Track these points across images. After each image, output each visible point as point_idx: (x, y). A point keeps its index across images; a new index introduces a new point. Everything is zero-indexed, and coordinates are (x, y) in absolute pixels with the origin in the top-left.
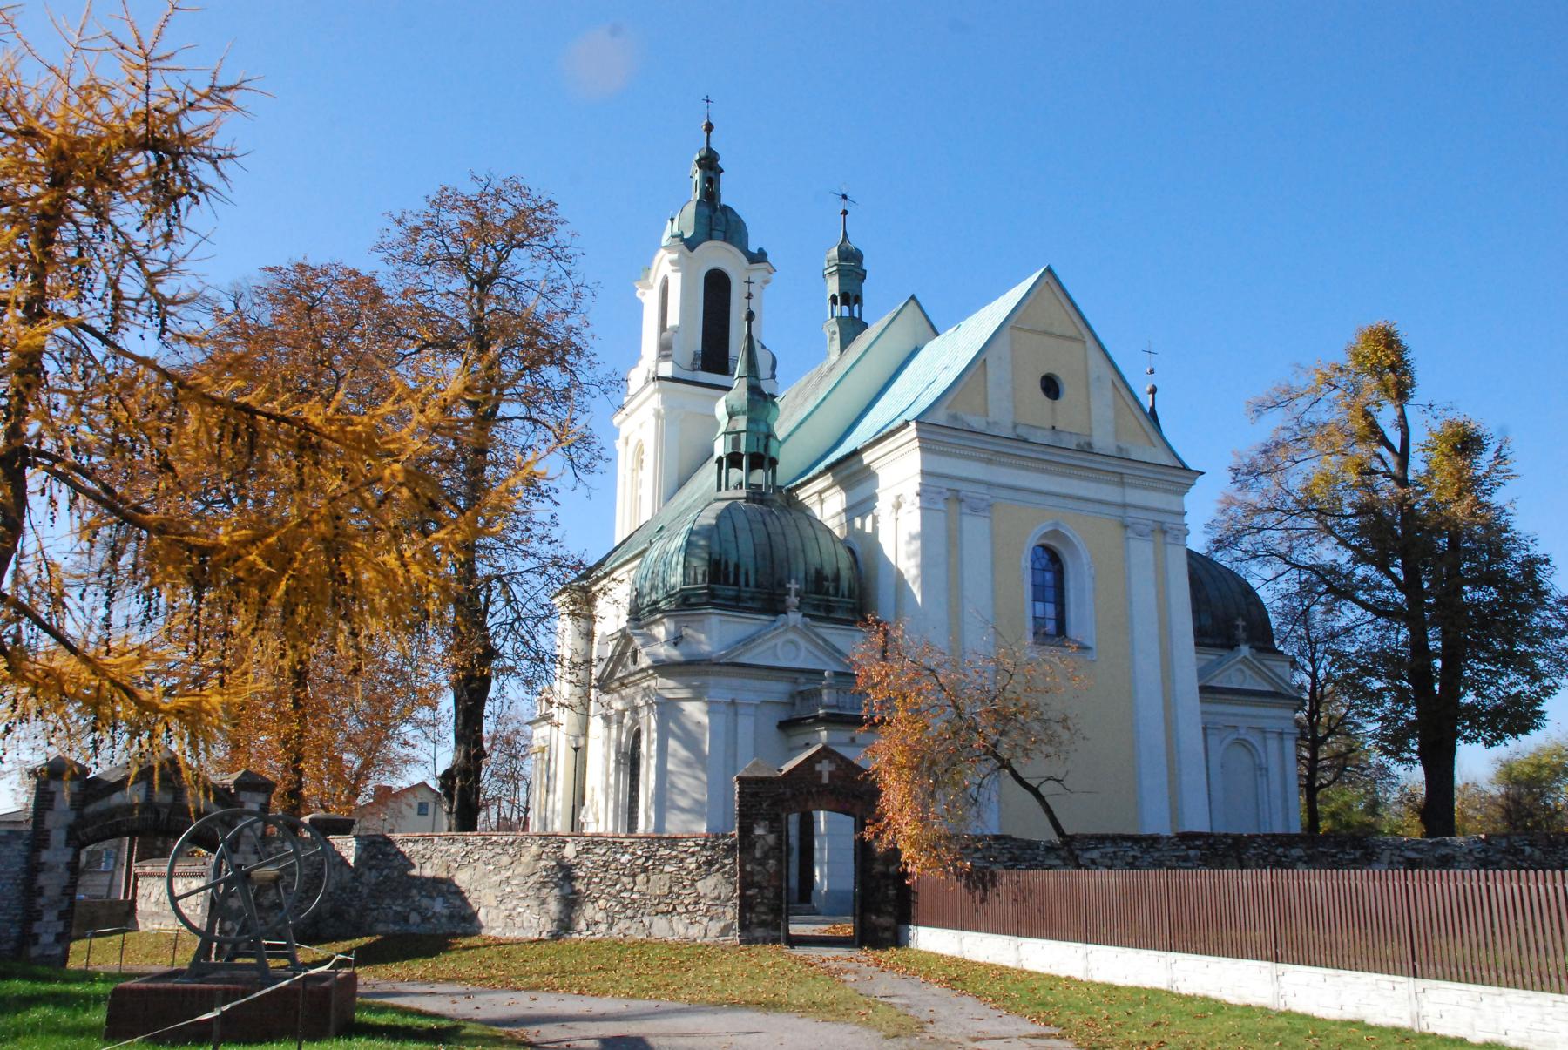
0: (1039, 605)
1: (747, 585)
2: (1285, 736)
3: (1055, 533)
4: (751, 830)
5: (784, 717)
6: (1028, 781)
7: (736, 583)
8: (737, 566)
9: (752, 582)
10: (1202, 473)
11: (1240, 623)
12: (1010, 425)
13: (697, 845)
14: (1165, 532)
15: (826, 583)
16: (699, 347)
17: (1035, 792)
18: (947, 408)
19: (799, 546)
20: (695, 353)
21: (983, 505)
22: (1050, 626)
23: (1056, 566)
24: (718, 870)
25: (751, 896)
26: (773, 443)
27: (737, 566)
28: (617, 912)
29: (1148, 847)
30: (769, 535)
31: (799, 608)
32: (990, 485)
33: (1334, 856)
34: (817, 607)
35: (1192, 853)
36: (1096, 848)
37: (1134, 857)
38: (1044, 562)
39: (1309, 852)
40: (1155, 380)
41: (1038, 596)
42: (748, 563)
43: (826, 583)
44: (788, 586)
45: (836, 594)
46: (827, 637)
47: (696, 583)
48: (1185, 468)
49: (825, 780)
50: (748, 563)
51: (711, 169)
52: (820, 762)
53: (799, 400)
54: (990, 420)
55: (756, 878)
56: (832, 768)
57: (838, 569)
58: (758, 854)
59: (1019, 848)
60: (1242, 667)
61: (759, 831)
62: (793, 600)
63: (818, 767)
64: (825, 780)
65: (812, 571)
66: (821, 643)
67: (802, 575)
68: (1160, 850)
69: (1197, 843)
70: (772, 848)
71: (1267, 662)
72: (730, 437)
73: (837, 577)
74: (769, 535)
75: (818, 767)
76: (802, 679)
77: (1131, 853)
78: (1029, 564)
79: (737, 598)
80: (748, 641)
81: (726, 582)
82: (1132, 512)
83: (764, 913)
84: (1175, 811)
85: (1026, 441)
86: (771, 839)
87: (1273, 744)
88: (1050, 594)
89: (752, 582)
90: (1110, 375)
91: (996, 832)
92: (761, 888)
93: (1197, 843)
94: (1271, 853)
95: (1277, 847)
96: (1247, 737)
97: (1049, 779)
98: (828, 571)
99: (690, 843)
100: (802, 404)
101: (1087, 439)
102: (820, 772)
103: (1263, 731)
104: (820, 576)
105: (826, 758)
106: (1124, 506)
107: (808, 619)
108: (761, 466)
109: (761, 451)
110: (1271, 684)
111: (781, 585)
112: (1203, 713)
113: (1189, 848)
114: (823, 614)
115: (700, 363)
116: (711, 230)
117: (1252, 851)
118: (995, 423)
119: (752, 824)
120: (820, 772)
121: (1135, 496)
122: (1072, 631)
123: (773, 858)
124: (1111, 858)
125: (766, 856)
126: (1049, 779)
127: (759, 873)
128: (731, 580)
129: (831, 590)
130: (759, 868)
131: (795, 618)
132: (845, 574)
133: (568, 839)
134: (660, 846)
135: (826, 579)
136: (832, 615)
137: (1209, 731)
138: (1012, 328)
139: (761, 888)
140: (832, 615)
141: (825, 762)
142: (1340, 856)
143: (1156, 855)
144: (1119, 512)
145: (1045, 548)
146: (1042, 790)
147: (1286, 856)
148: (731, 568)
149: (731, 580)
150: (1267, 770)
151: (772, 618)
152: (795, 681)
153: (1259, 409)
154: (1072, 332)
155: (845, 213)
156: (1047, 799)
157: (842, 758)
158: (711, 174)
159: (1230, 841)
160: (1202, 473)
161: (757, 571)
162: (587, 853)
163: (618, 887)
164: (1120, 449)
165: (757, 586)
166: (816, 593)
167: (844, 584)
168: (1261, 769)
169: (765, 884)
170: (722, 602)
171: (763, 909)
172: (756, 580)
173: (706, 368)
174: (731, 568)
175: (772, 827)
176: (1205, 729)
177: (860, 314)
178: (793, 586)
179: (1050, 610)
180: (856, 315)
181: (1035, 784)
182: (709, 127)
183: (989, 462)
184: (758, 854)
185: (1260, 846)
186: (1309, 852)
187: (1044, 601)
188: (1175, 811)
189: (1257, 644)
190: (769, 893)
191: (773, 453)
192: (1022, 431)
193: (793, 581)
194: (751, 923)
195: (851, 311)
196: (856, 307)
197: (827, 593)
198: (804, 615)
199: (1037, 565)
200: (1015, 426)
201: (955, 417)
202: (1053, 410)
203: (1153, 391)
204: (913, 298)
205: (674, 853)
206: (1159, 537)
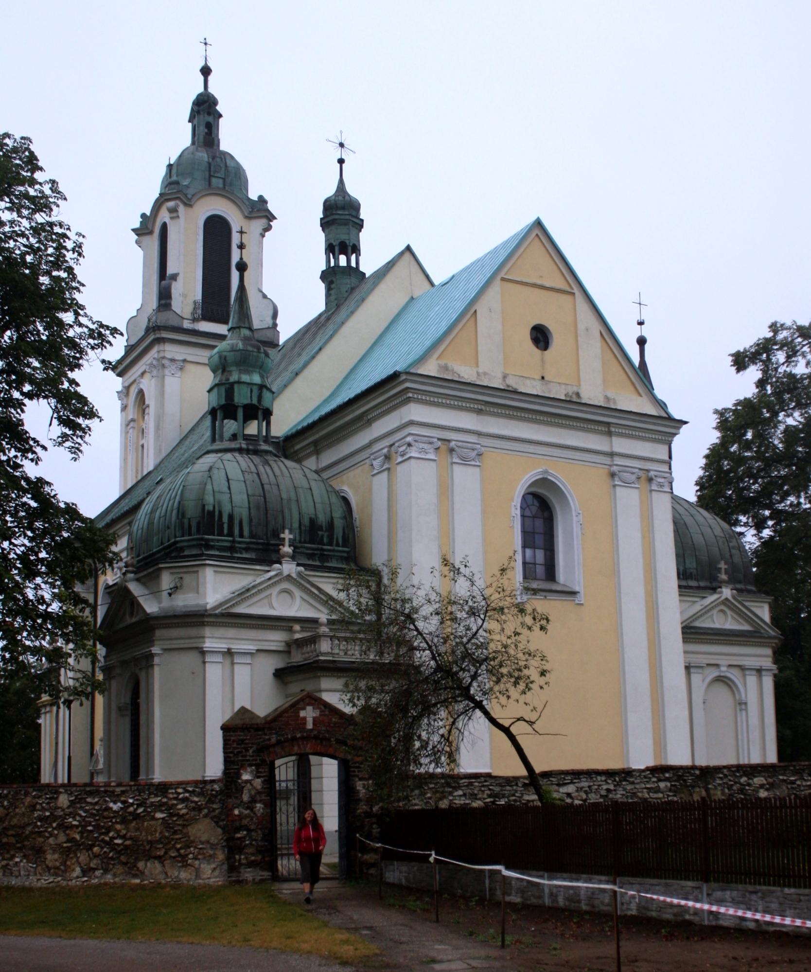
0: (529, 552)
1: (241, 535)
2: (764, 673)
3: (544, 481)
4: (239, 776)
5: (281, 665)
6: (501, 721)
7: (231, 533)
8: (231, 517)
9: (246, 532)
10: (686, 423)
11: (722, 565)
12: (500, 376)
13: (188, 791)
14: (650, 480)
15: (320, 533)
16: (199, 296)
17: (506, 731)
18: (437, 359)
19: (293, 496)
20: (195, 303)
21: (473, 454)
22: (540, 571)
23: (546, 514)
24: (206, 816)
25: (239, 839)
26: (266, 395)
27: (231, 517)
28: (112, 858)
29: (621, 781)
30: (262, 485)
31: (293, 558)
32: (479, 434)
33: (793, 782)
34: (311, 556)
35: (662, 785)
36: (572, 783)
37: (608, 790)
38: (534, 509)
39: (770, 780)
40: (646, 331)
41: (528, 541)
42: (242, 512)
43: (320, 533)
44: (282, 536)
45: (330, 544)
46: (321, 586)
47: (190, 535)
48: (670, 418)
49: (310, 726)
50: (242, 512)
51: (209, 114)
52: (304, 709)
53: (296, 350)
54: (481, 371)
55: (245, 822)
56: (317, 713)
57: (332, 518)
58: (246, 798)
59: (500, 785)
60: (722, 607)
61: (246, 777)
62: (287, 549)
63: (302, 714)
64: (310, 726)
65: (306, 522)
66: (316, 592)
67: (296, 525)
68: (633, 783)
69: (667, 775)
70: (259, 793)
71: (747, 604)
72: (223, 389)
73: (331, 525)
74: (262, 485)
75: (302, 714)
76: (297, 627)
77: (605, 787)
78: (518, 512)
79: (232, 549)
80: (244, 594)
81: (221, 534)
82: (618, 461)
83: (253, 854)
84: (660, 743)
85: (515, 392)
86: (258, 783)
87: (752, 680)
88: (539, 540)
89: (246, 532)
90: (596, 327)
91: (651, 763)
92: (249, 830)
93: (667, 775)
94: (736, 783)
95: (741, 777)
96: (728, 675)
97: (518, 720)
98: (322, 519)
99: (180, 790)
100: (300, 355)
101: (575, 389)
102: (305, 719)
103: (742, 668)
104: (313, 524)
105: (309, 704)
106: (612, 455)
107: (301, 569)
108: (255, 417)
109: (255, 402)
110: (751, 624)
111: (276, 534)
112: (685, 652)
113: (660, 780)
114: (317, 563)
115: (199, 312)
116: (210, 176)
117: (719, 781)
118: (485, 373)
119: (239, 770)
120: (305, 719)
121: (621, 445)
122: (562, 575)
123: (260, 801)
124: (586, 792)
125: (253, 800)
126: (518, 720)
127: (246, 816)
128: (226, 531)
129: (325, 540)
130: (247, 812)
131: (289, 568)
132: (339, 524)
133: (61, 790)
134: (150, 794)
135: (320, 528)
136: (326, 564)
137: (692, 670)
138: (503, 279)
139: (249, 830)
140: (326, 564)
141: (309, 708)
142: (798, 782)
143: (629, 787)
144: (607, 460)
145: (535, 495)
146: (513, 730)
147: (749, 785)
148: (225, 519)
149: (226, 531)
150: (746, 704)
151: (267, 568)
152: (290, 630)
153: (740, 361)
154: (563, 286)
155: (341, 161)
156: (518, 738)
157: (326, 705)
158: (210, 119)
159: (697, 772)
160: (686, 423)
161: (251, 520)
162: (79, 803)
163: (111, 834)
164: (607, 399)
165: (252, 536)
166: (309, 543)
167: (339, 532)
168: (740, 704)
169: (253, 827)
170: (217, 553)
171: (251, 850)
172: (251, 532)
173: (207, 317)
174: (225, 519)
175: (258, 772)
176: (688, 668)
177: (357, 263)
178: (287, 535)
179: (540, 556)
180: (353, 264)
181: (506, 723)
182: (206, 71)
183: (479, 412)
184: (246, 798)
185: (726, 776)
186: (770, 780)
187: (534, 547)
188: (660, 743)
189: (738, 586)
190: (258, 835)
191: (266, 403)
192: (513, 382)
193: (287, 531)
194: (241, 864)
195: (349, 261)
196: (353, 257)
197: (321, 543)
198: (298, 565)
199: (528, 513)
200: (505, 377)
201: (446, 368)
202: (543, 361)
203: (642, 342)
204: (408, 248)
205: (165, 800)
206: (643, 485)
